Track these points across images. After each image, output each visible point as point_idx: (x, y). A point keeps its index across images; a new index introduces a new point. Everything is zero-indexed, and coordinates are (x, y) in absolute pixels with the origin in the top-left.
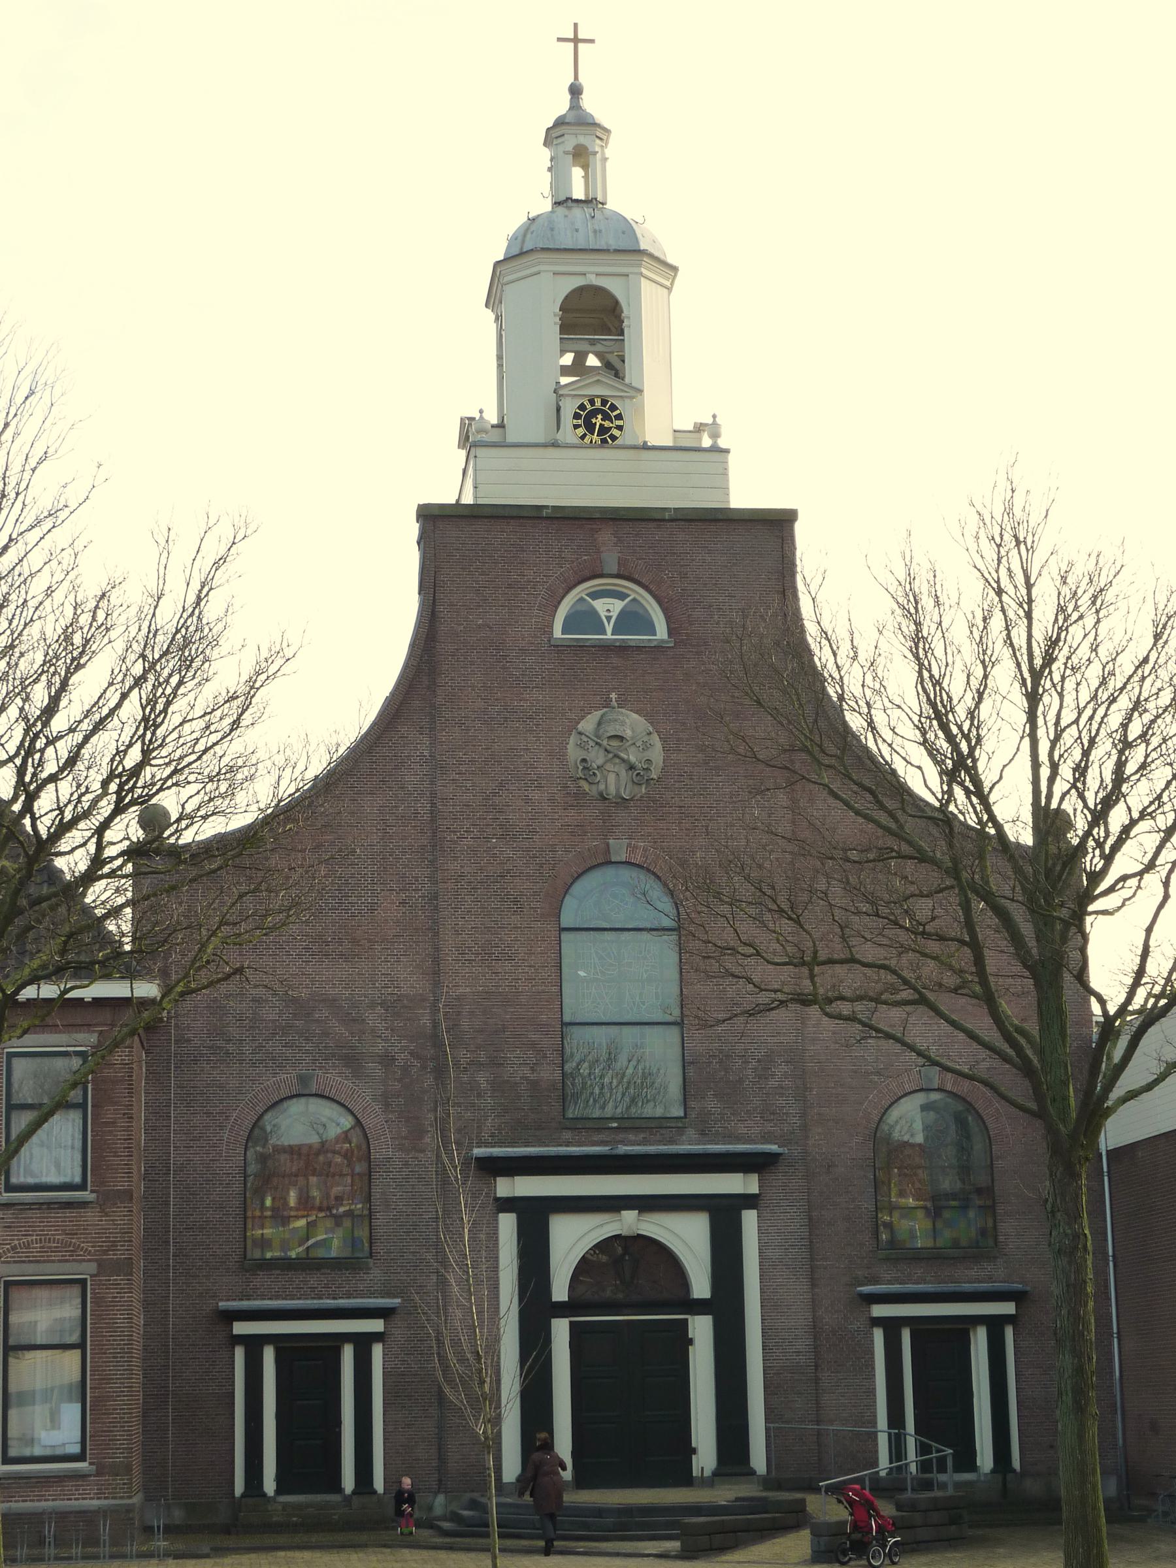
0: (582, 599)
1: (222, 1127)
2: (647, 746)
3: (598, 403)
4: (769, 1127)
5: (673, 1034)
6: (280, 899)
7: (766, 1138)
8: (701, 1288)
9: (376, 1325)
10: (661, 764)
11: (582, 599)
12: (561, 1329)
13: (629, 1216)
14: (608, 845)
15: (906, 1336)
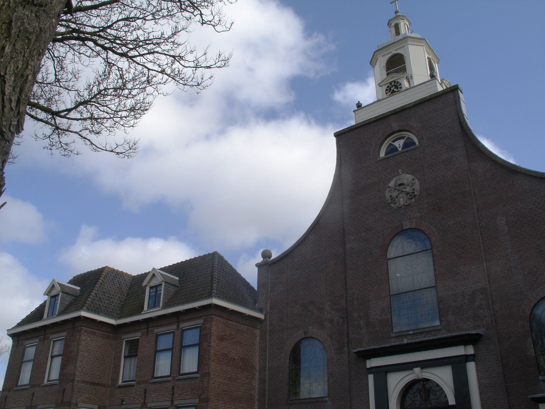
0: (390, 144)
1: (282, 353)
2: (413, 184)
3: (393, 84)
6: (129, 103)
7: (475, 328)
10: (419, 189)
11: (390, 144)
13: (417, 370)
14: (402, 224)
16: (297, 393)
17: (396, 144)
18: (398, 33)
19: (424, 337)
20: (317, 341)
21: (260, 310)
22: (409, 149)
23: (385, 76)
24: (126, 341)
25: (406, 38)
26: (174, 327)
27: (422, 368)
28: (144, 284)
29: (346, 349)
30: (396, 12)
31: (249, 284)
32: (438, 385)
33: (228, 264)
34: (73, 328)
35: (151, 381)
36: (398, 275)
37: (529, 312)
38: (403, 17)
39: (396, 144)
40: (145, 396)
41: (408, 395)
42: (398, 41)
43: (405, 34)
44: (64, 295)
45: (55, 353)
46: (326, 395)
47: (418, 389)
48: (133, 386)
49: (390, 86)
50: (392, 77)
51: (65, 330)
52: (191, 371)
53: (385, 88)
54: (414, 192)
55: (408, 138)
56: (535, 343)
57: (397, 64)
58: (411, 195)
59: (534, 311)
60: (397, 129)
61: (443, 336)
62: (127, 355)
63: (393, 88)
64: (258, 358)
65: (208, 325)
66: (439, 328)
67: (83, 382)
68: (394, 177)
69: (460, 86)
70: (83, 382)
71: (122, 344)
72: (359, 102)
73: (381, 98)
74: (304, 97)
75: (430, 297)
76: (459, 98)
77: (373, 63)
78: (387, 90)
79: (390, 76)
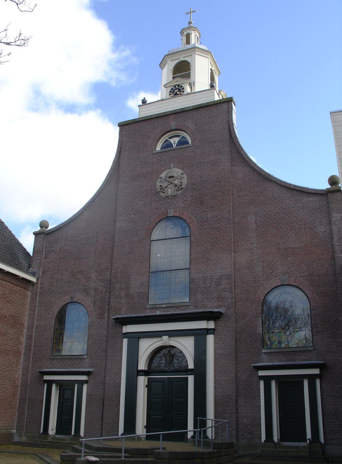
0: (167, 140)
1: (49, 314)
2: (182, 178)
3: (177, 87)
4: (220, 303)
5: (187, 273)
8: (191, 366)
9: (84, 378)
10: (186, 183)
12: (142, 381)
13: (165, 338)
15: (273, 384)
16: (59, 350)
17: (172, 141)
18: (188, 42)
19: (175, 311)
20: (79, 305)
21: (34, 274)
22: (182, 146)
23: (171, 79)
25: (195, 48)
27: (169, 337)
29: (106, 315)
30: (190, 23)
31: (25, 249)
32: (181, 352)
33: (8, 229)
36: (159, 255)
37: (263, 298)
38: (195, 29)
39: (172, 141)
41: (156, 358)
42: (187, 49)
43: (195, 44)
46: (85, 353)
47: (164, 354)
49: (174, 88)
50: (177, 81)
53: (169, 89)
54: (181, 185)
55: (183, 137)
56: (263, 323)
57: (183, 69)
58: (179, 187)
59: (266, 297)
60: (174, 128)
61: (191, 311)
63: (176, 91)
64: (27, 317)
66: (188, 304)
68: (166, 169)
69: (235, 99)
72: (144, 98)
73: (164, 98)
74: (103, 95)
75: (184, 276)
76: (232, 109)
77: (162, 65)
78: (170, 92)
79: (175, 80)
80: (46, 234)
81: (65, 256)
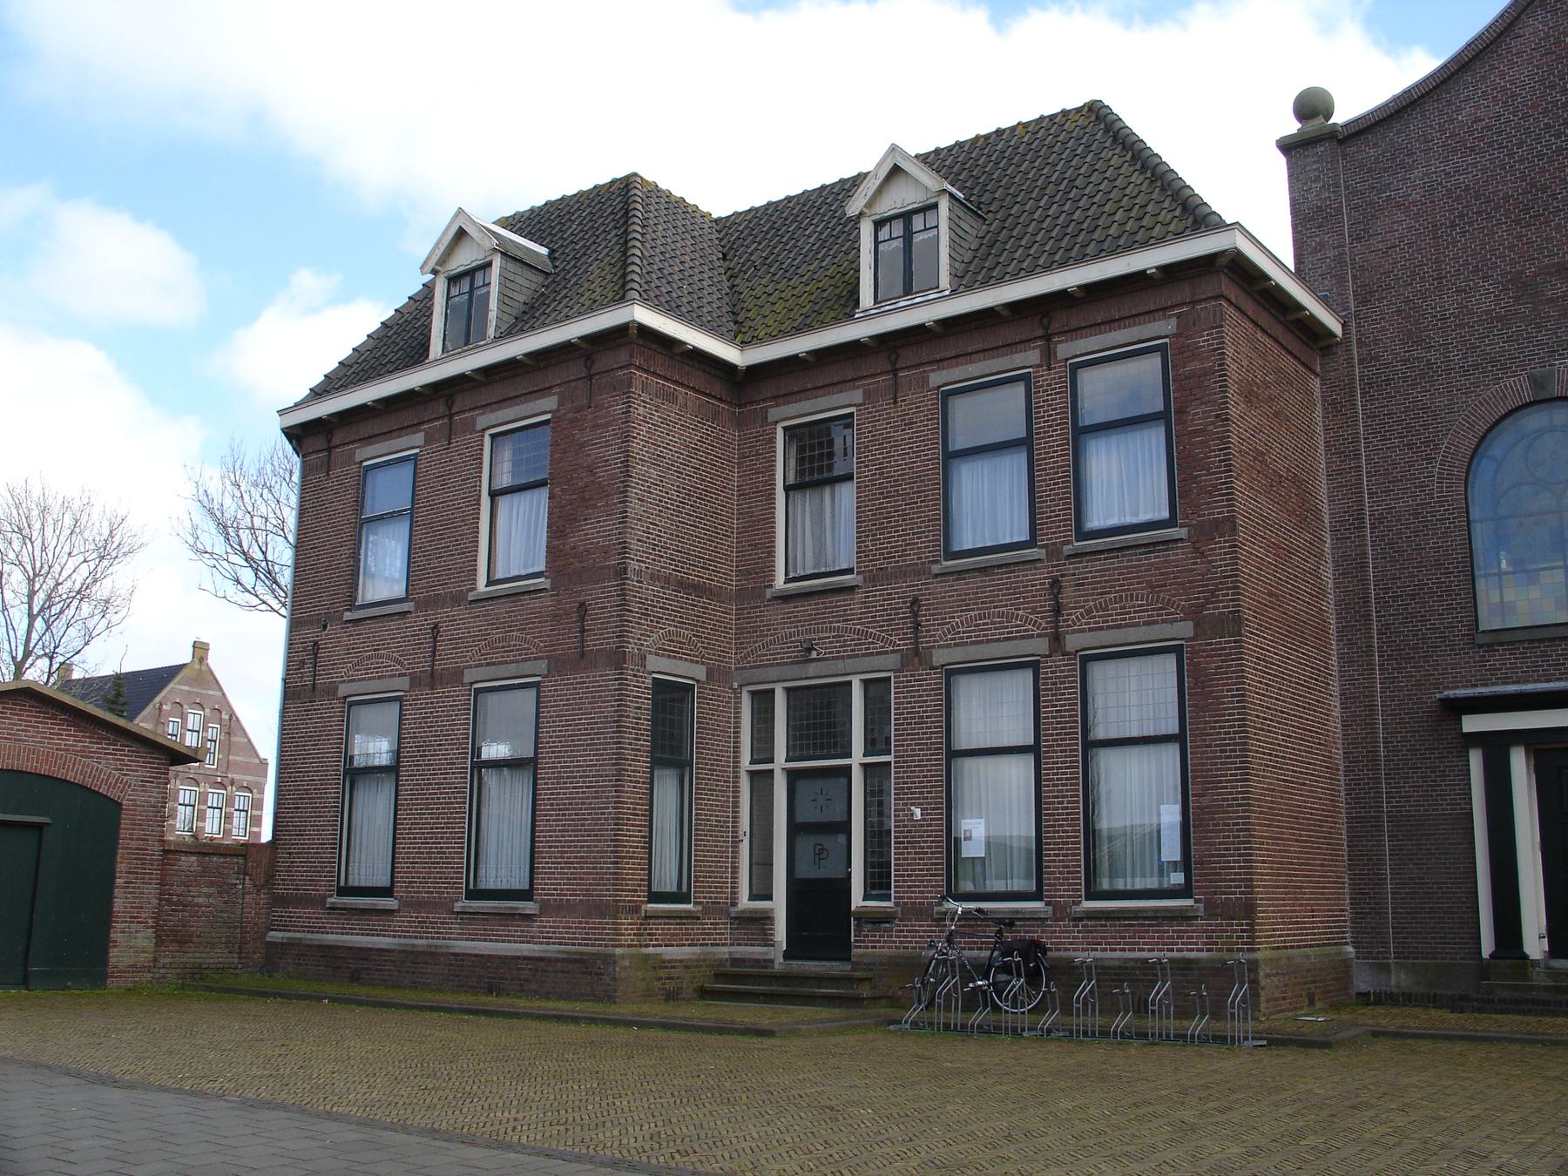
1: (1430, 460)
24: (785, 428)
26: (1032, 356)
28: (853, 208)
34: (590, 377)
35: (936, 569)
40: (917, 626)
44: (511, 266)
45: (505, 480)
48: (850, 589)
51: (545, 391)
52: (1130, 520)
62: (791, 480)
65: (1203, 340)
67: (654, 577)
70: (654, 577)
71: (772, 441)
80: (1341, 142)
81: (1461, 216)
